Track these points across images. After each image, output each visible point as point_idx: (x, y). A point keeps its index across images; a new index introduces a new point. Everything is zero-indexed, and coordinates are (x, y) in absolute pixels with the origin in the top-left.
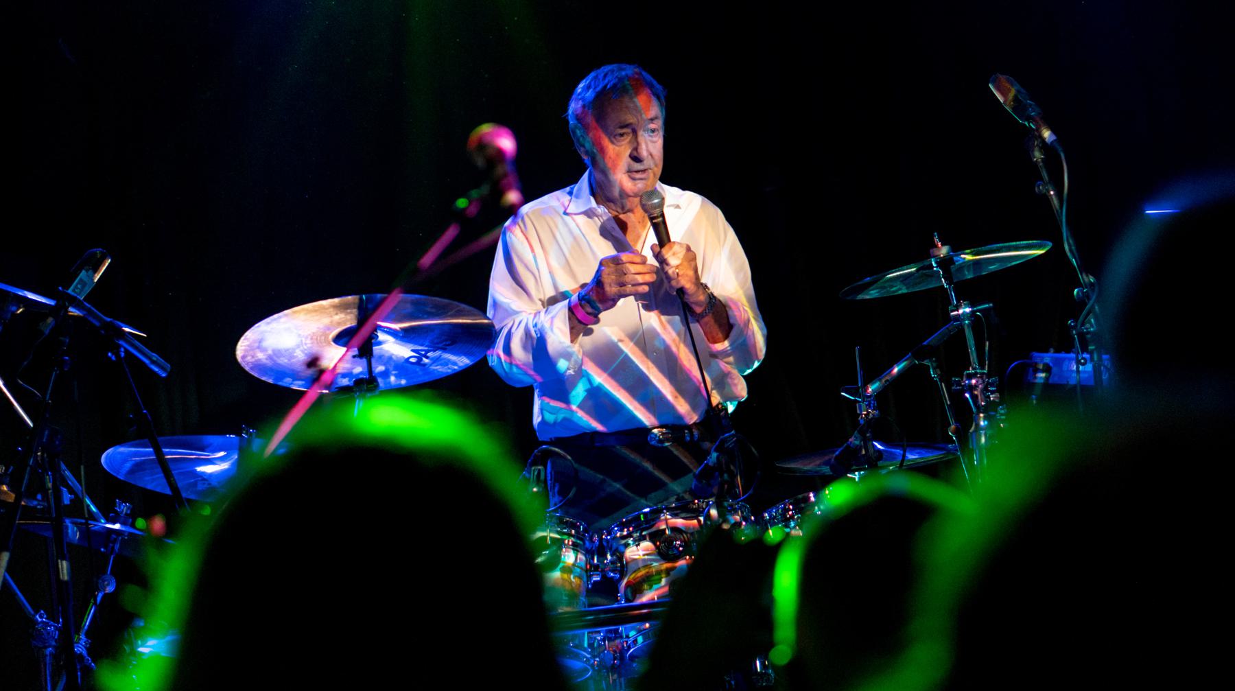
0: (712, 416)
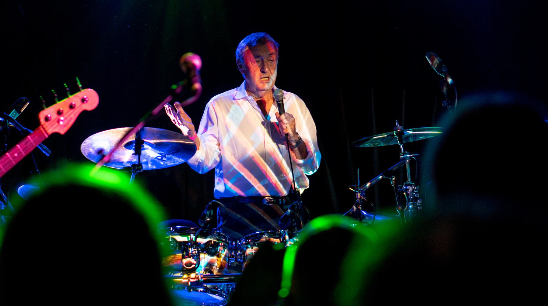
0: (293, 193)
